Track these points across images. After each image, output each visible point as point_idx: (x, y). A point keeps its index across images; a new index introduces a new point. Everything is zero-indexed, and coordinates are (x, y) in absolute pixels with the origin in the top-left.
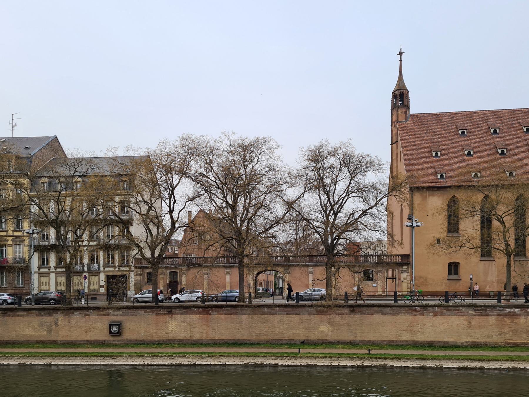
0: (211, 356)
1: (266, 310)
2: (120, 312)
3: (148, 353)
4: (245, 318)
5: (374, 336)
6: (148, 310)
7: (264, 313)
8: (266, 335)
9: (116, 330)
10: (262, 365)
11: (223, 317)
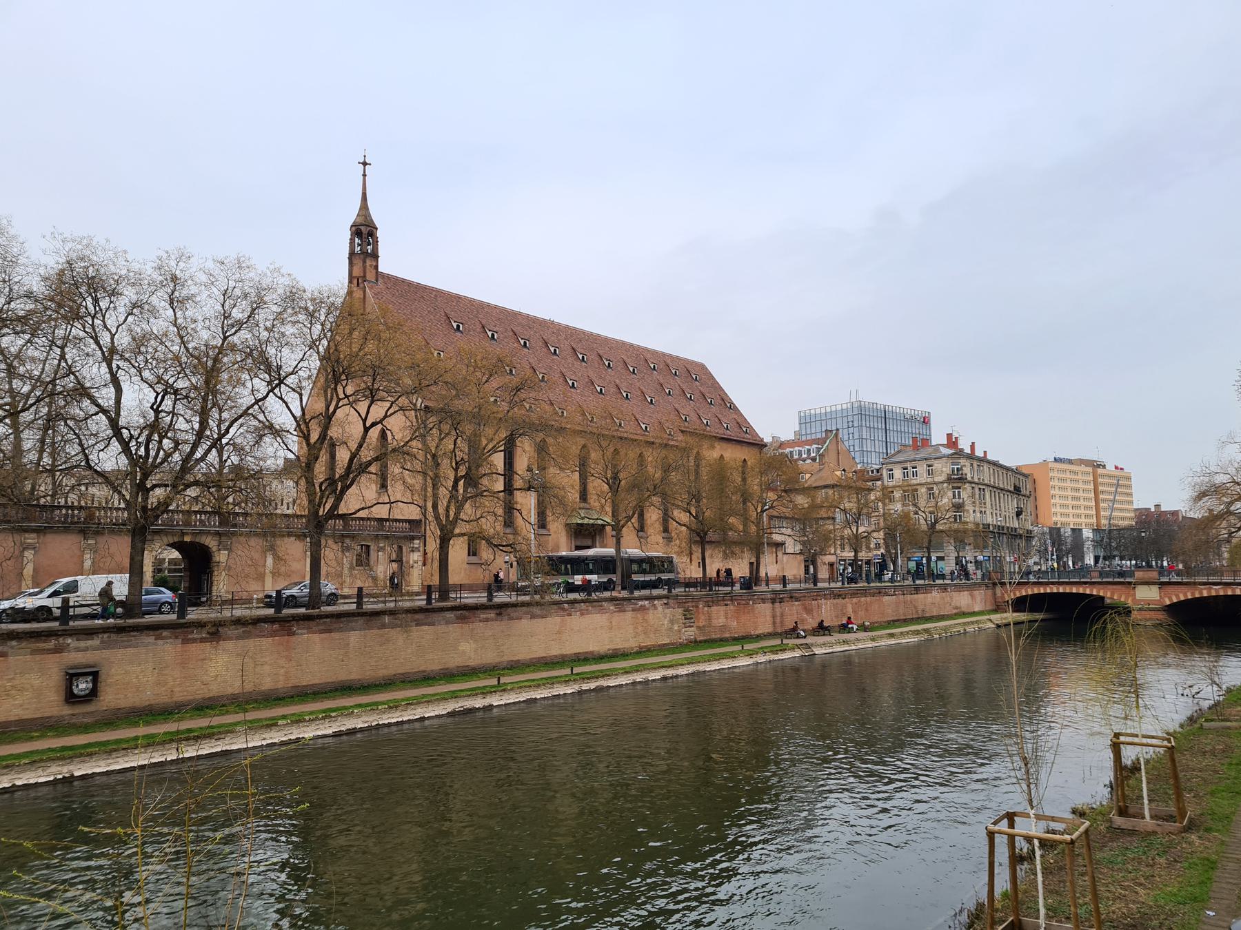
0: (394, 706)
1: (387, 619)
2: (95, 642)
3: (284, 717)
4: (355, 637)
5: (523, 654)
6: (165, 633)
7: (383, 626)
8: (386, 668)
9: (82, 687)
10: (473, 710)
11: (316, 637)
